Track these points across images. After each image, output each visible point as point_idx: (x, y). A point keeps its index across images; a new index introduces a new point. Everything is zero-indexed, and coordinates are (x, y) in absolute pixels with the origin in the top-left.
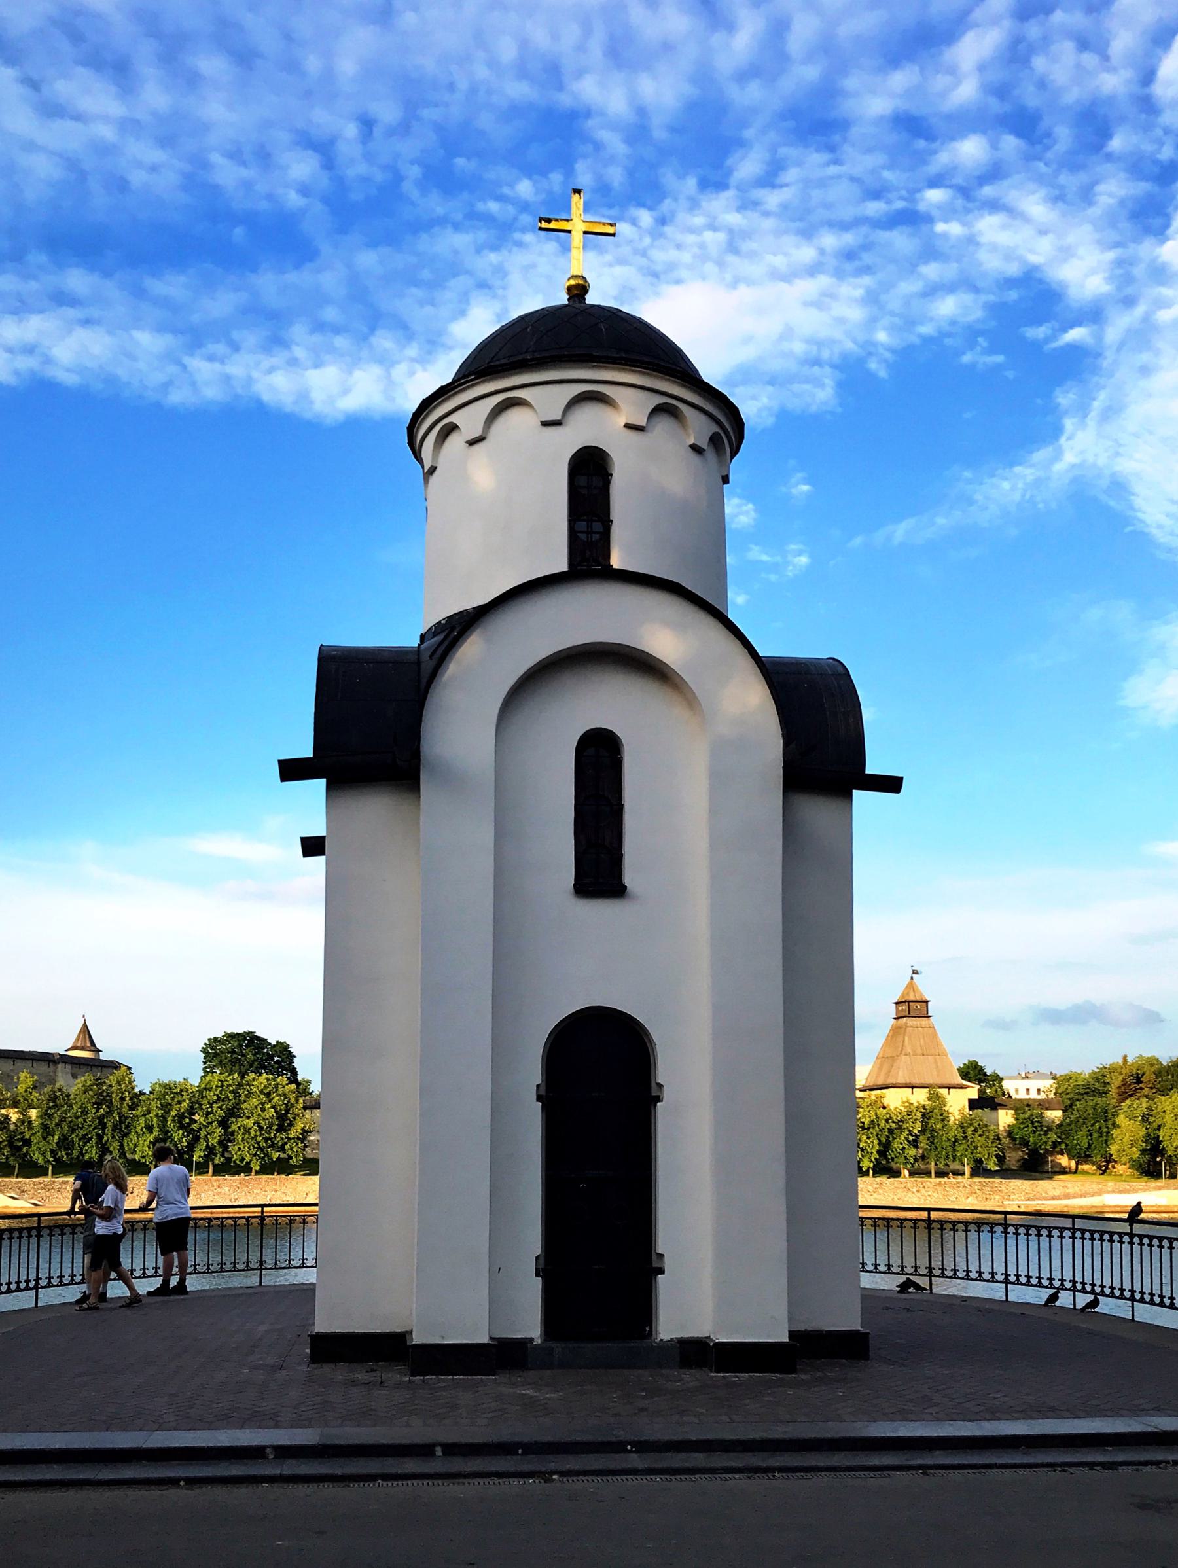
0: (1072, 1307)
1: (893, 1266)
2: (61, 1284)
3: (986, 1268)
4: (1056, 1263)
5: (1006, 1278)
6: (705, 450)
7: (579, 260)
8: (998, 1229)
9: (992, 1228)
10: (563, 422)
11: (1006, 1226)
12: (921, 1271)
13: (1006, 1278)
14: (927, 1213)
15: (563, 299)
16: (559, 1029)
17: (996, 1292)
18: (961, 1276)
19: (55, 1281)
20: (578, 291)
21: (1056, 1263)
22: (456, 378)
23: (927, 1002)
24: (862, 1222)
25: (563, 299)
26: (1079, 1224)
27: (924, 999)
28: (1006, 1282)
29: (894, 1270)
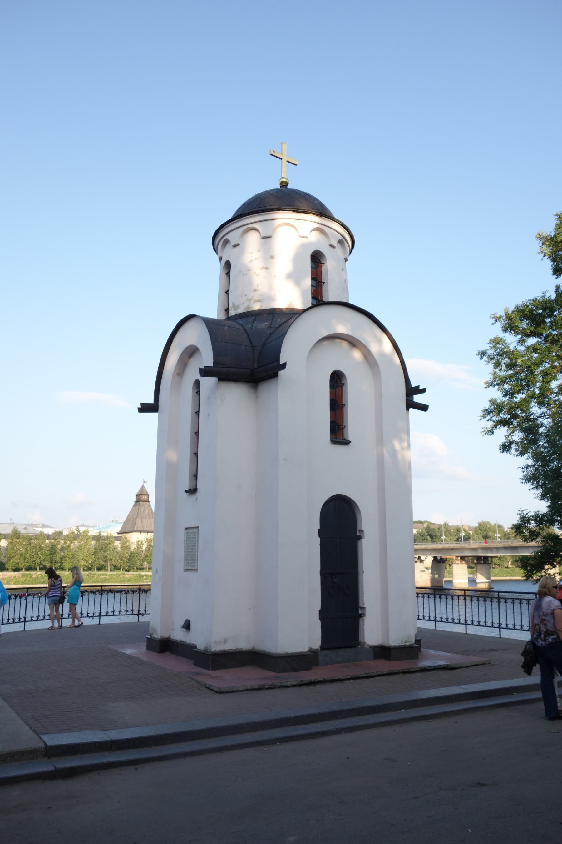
0: (499, 636)
1: (516, 625)
2: (14, 622)
3: (518, 623)
4: (426, 610)
5: (435, 619)
6: (336, 247)
7: (285, 171)
8: (462, 598)
9: (446, 597)
10: (272, 236)
11: (465, 597)
12: (517, 627)
13: (435, 619)
14: (464, 591)
15: (278, 186)
16: (333, 498)
17: (459, 629)
18: (444, 621)
19: (11, 621)
20: (284, 184)
21: (426, 610)
22: (235, 216)
23: (148, 495)
24: (418, 595)
25: (278, 186)
26: (467, 593)
27: (147, 494)
28: (466, 624)
29: (517, 627)
